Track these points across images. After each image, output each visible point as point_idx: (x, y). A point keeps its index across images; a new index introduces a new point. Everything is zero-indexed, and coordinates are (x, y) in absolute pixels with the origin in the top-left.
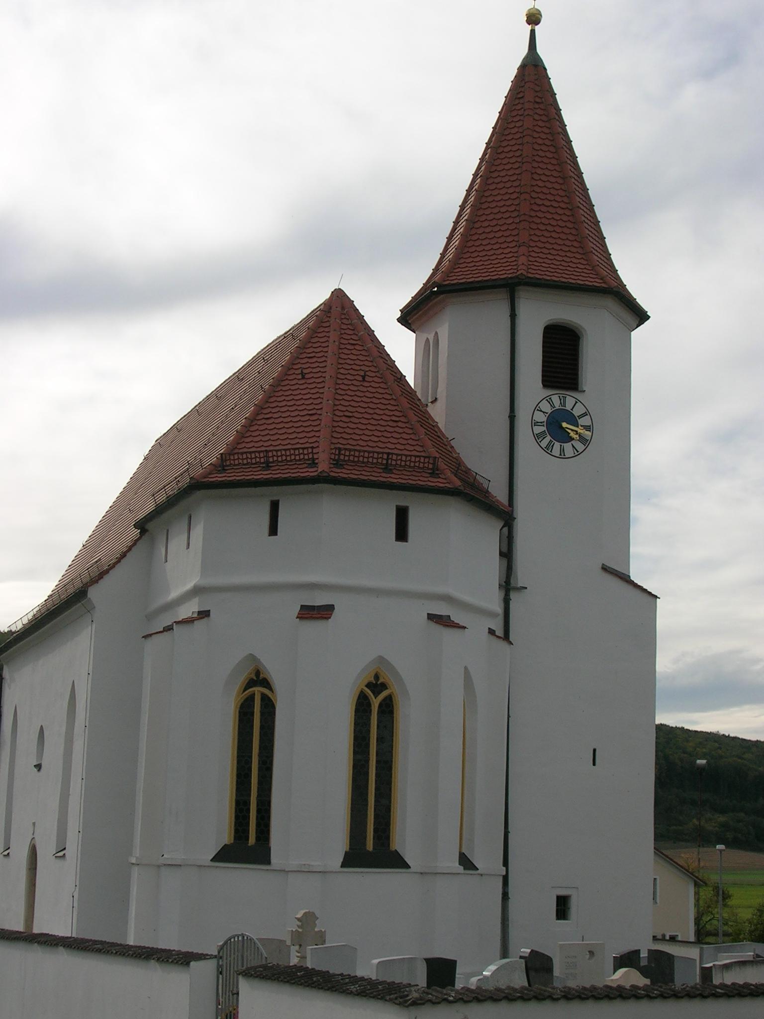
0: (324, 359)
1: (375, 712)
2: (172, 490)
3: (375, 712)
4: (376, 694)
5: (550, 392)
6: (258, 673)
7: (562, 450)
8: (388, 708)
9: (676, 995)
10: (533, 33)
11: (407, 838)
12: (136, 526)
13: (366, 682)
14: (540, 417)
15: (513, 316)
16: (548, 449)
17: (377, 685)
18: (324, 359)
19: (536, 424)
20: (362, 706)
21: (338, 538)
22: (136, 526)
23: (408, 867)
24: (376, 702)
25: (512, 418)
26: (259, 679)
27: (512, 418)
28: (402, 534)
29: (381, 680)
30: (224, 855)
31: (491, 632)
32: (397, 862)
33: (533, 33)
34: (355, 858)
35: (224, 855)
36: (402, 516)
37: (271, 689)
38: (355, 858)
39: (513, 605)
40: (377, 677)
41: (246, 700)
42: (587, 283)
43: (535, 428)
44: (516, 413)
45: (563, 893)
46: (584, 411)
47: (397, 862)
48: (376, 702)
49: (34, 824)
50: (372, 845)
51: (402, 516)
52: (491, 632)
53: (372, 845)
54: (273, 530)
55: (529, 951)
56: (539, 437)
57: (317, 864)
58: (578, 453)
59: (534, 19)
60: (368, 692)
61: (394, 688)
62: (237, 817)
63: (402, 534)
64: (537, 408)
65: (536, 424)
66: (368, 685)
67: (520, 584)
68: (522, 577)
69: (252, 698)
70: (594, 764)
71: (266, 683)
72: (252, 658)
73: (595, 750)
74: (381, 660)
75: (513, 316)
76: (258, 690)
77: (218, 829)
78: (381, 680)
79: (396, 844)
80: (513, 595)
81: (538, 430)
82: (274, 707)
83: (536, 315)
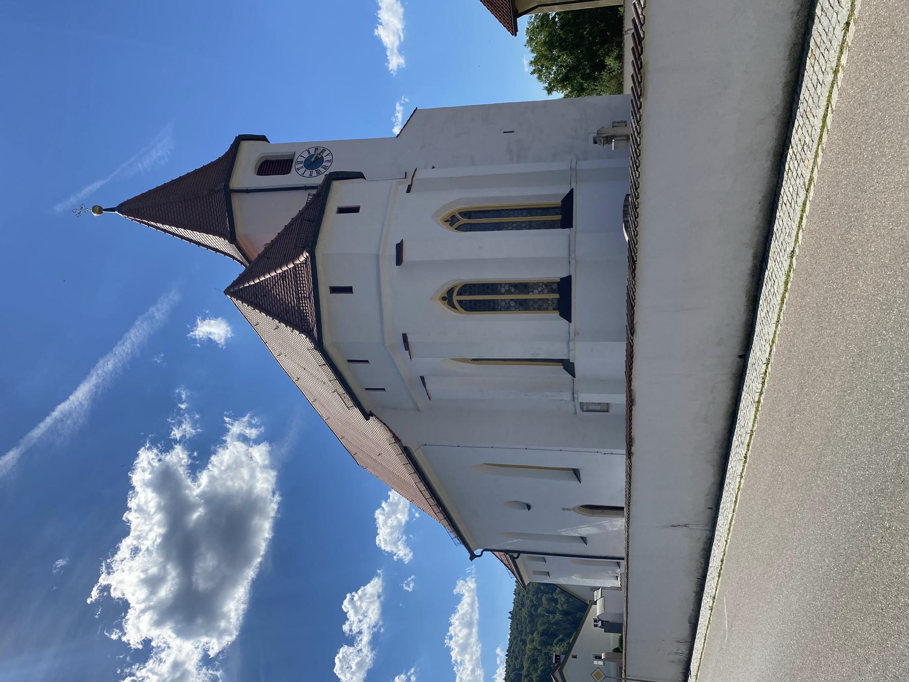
1: (471, 220)
2: (450, 528)
5: (293, 169)
6: (444, 299)
7: (328, 161)
9: (629, 504)
10: (105, 210)
11: (553, 194)
12: (367, 419)
14: (308, 172)
15: (248, 191)
17: (451, 221)
19: (311, 175)
22: (367, 419)
33: (105, 210)
35: (565, 311)
49: (564, 509)
54: (349, 290)
59: (100, 210)
60: (456, 225)
66: (451, 225)
69: (460, 302)
71: (450, 292)
75: (248, 191)
76: (456, 298)
79: (558, 202)
82: (465, 286)
83: (244, 175)
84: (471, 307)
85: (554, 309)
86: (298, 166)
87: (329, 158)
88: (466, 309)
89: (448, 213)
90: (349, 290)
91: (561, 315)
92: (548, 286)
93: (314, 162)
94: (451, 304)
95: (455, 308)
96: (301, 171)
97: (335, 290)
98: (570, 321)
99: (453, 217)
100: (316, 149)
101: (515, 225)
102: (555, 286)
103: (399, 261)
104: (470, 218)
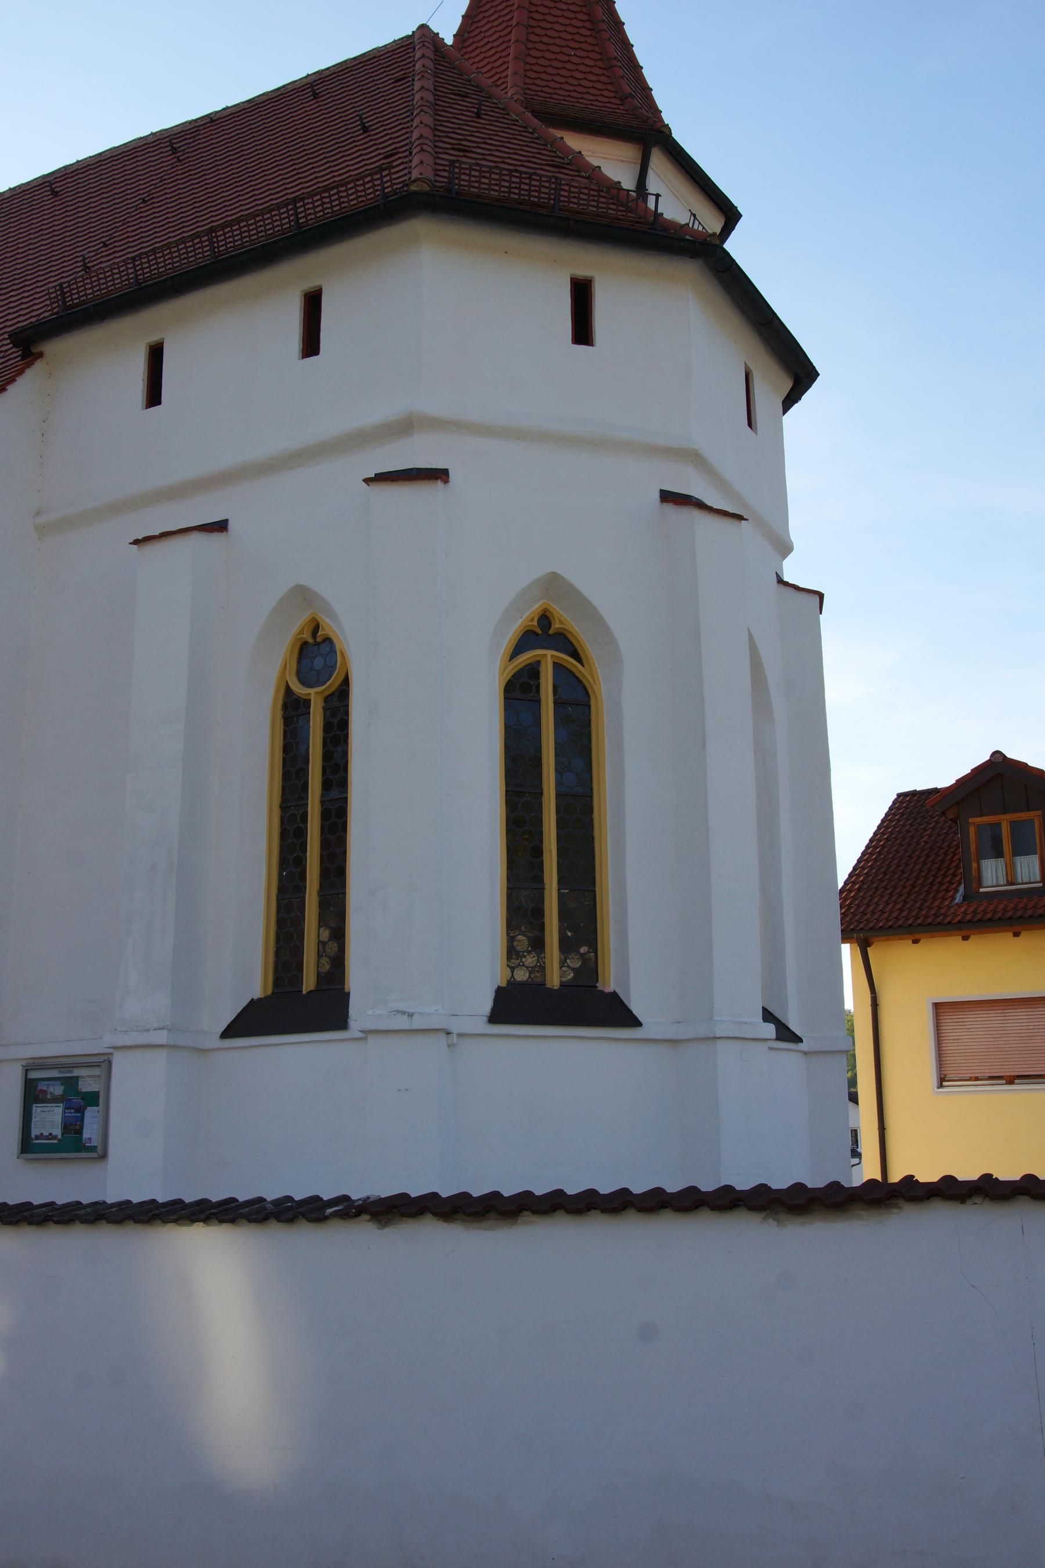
0: (505, 66)
1: (550, 704)
3: (550, 704)
6: (316, 628)
11: (637, 960)
17: (544, 633)
18: (505, 66)
20: (520, 690)
23: (634, 1022)
28: (583, 332)
29: (556, 626)
30: (251, 1022)
32: (616, 1013)
34: (519, 1004)
35: (251, 1022)
36: (582, 294)
37: (576, 655)
38: (519, 1004)
42: (20, 325)
47: (616, 1013)
50: (559, 980)
51: (582, 294)
53: (559, 980)
55: (846, 949)
57: (431, 1012)
62: (284, 835)
63: (583, 332)
72: (301, 594)
74: (553, 583)
77: (242, 972)
89: (566, 618)
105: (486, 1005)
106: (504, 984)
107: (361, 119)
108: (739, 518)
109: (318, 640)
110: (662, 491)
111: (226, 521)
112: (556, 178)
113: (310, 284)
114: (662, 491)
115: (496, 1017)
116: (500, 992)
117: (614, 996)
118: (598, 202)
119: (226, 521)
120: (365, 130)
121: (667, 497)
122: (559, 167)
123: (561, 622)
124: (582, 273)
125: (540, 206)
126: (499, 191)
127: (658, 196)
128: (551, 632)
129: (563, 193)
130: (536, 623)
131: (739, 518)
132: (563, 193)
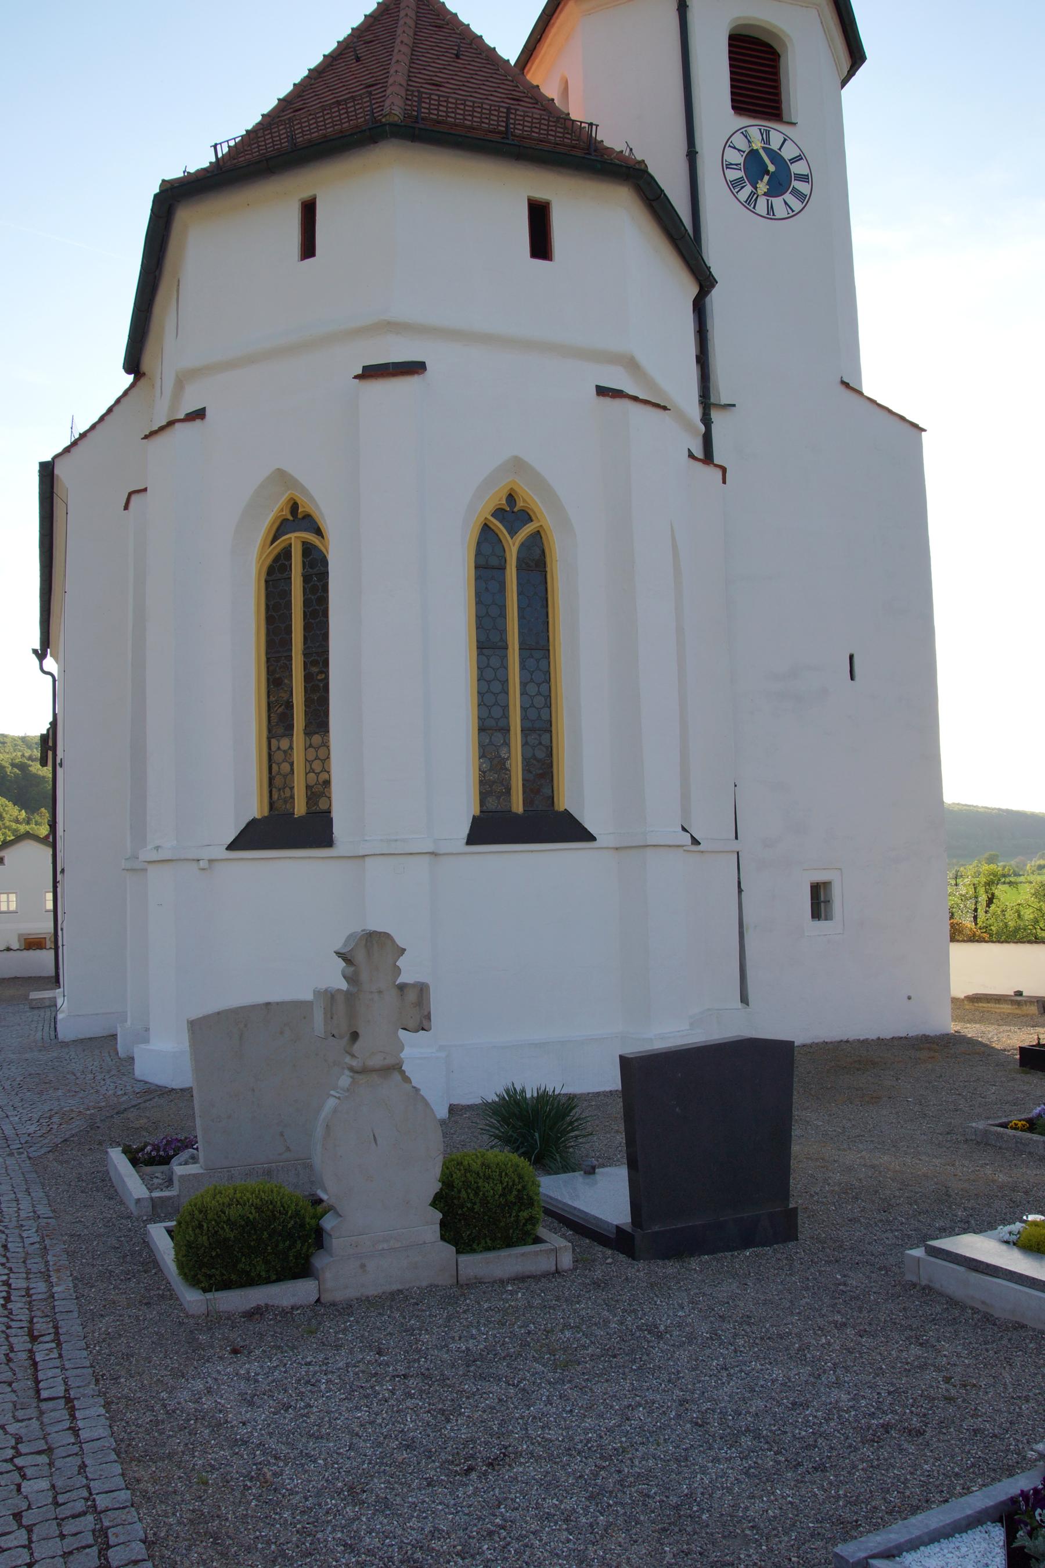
1: (513, 571)
3: (513, 571)
4: (513, 533)
5: (744, 121)
6: (294, 507)
7: (770, 208)
8: (536, 563)
11: (585, 787)
13: (491, 508)
14: (738, 159)
16: (751, 202)
17: (512, 512)
19: (729, 166)
21: (422, 223)
23: (591, 838)
24: (512, 547)
25: (692, 155)
26: (298, 518)
27: (692, 155)
28: (541, 245)
29: (520, 504)
30: (252, 837)
31: (691, 455)
34: (490, 828)
35: (252, 837)
36: (539, 216)
37: (319, 532)
38: (490, 828)
39: (715, 428)
40: (511, 498)
41: (277, 559)
43: (728, 172)
44: (698, 148)
45: (820, 877)
46: (797, 153)
48: (512, 547)
51: (539, 216)
52: (691, 455)
56: (735, 185)
58: (793, 214)
60: (497, 525)
61: (546, 518)
63: (541, 245)
64: (728, 144)
65: (729, 166)
66: (499, 513)
67: (724, 401)
68: (723, 390)
69: (286, 554)
70: (852, 678)
72: (282, 477)
73: (851, 657)
74: (518, 465)
76: (295, 539)
78: (520, 504)
79: (565, 801)
80: (715, 415)
81: (733, 175)
82: (325, 562)
84: (487, 566)
85: (272, 805)
86: (754, 133)
87: (780, 210)
88: (270, 571)
89: (531, 497)
90: (308, 249)
91: (252, 824)
92: (320, 790)
93: (770, 177)
94: (281, 528)
95: (272, 543)
96: (739, 141)
97: (309, 210)
98: (231, 847)
99: (526, 516)
100: (804, 178)
101: (496, 687)
102: (322, 805)
103: (371, 373)
104: (523, 565)
105: (465, 830)
106: (478, 813)
107: (355, 51)
108: (665, 408)
109: (300, 516)
110: (597, 387)
111: (204, 409)
112: (418, 91)
113: (306, 195)
114: (597, 387)
115: (471, 840)
116: (475, 821)
117: (567, 814)
118: (490, 119)
119: (204, 409)
120: (358, 60)
121: (602, 391)
122: (437, 85)
123: (524, 501)
124: (541, 195)
125: (530, 139)
126: (555, 136)
127: (597, 126)
128: (516, 510)
129: (424, 105)
130: (504, 502)
131: (665, 408)
132: (424, 105)
